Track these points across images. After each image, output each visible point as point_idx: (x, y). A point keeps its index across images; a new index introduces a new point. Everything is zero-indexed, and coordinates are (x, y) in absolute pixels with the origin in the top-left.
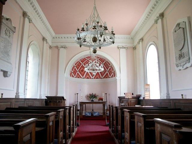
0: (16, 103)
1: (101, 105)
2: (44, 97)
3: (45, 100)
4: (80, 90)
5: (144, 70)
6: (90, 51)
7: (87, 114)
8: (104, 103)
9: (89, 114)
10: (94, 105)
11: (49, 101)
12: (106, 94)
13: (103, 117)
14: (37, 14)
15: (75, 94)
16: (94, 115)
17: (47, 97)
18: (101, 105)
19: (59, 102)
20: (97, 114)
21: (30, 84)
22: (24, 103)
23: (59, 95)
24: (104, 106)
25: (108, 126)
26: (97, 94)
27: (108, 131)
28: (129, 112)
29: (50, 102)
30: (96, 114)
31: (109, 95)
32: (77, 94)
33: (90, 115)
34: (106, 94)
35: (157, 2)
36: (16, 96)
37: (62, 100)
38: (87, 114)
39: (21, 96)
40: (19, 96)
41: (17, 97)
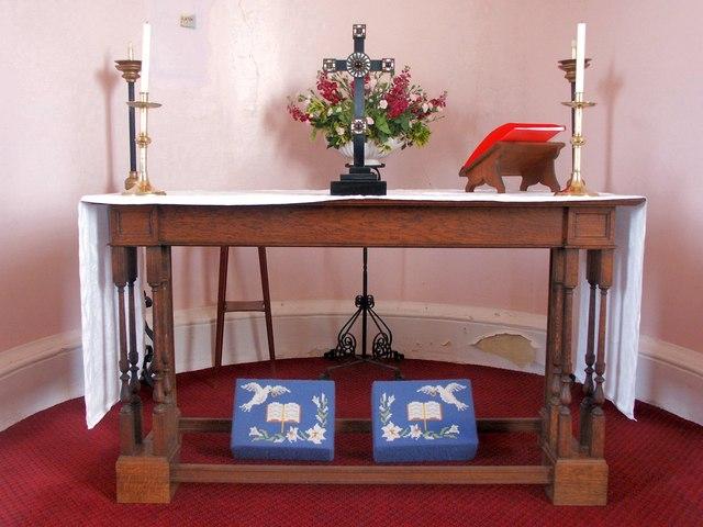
4: (188, 22)
7: (261, 410)
8: (586, 233)
15: (107, 81)
20: (432, 411)
26: (424, 83)
33: (318, 435)
38: (261, 410)
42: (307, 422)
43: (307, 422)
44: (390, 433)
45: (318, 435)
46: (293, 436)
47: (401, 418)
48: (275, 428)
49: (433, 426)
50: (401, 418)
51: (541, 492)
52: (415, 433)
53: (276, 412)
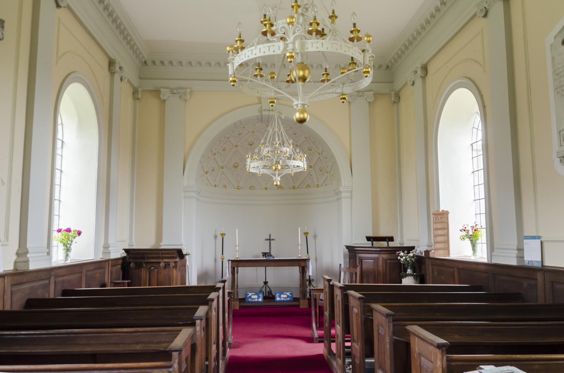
0: (16, 288)
1: (296, 270)
2: (117, 253)
3: (121, 261)
5: (78, 17)
6: (259, 106)
7: (250, 297)
8: (303, 264)
9: (256, 297)
10: (271, 270)
11: (136, 263)
12: (306, 234)
13: (301, 307)
14: (120, 33)
15: (216, 237)
16: (278, 299)
17: (126, 251)
18: (296, 270)
19: (167, 265)
20: (286, 296)
21: (76, 220)
22: (46, 282)
23: (167, 244)
24: (303, 270)
25: (322, 342)
27: (321, 356)
28: (387, 315)
29: (139, 266)
30: (282, 296)
31: (315, 237)
32: (223, 235)
33: (260, 300)
34: (306, 234)
35: (443, 3)
36: (16, 263)
37: (178, 260)
38: (250, 297)
39: (35, 264)
40: (27, 262)
41: (21, 268)
42: (259, 297)
43: (259, 297)
44: (278, 299)
45: (260, 300)
46: (256, 300)
47: (280, 297)
48: (253, 299)
49: (285, 298)
50: (280, 297)
51: (298, 306)
52: (282, 299)
53: (253, 297)
